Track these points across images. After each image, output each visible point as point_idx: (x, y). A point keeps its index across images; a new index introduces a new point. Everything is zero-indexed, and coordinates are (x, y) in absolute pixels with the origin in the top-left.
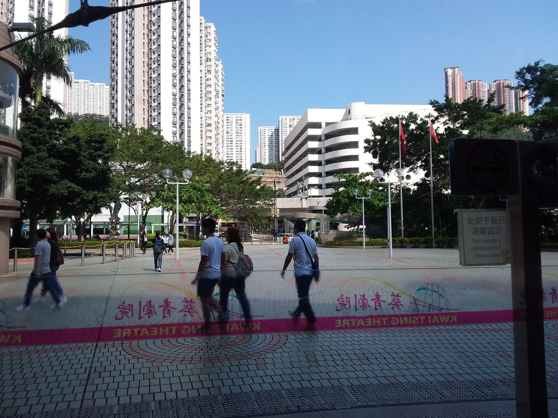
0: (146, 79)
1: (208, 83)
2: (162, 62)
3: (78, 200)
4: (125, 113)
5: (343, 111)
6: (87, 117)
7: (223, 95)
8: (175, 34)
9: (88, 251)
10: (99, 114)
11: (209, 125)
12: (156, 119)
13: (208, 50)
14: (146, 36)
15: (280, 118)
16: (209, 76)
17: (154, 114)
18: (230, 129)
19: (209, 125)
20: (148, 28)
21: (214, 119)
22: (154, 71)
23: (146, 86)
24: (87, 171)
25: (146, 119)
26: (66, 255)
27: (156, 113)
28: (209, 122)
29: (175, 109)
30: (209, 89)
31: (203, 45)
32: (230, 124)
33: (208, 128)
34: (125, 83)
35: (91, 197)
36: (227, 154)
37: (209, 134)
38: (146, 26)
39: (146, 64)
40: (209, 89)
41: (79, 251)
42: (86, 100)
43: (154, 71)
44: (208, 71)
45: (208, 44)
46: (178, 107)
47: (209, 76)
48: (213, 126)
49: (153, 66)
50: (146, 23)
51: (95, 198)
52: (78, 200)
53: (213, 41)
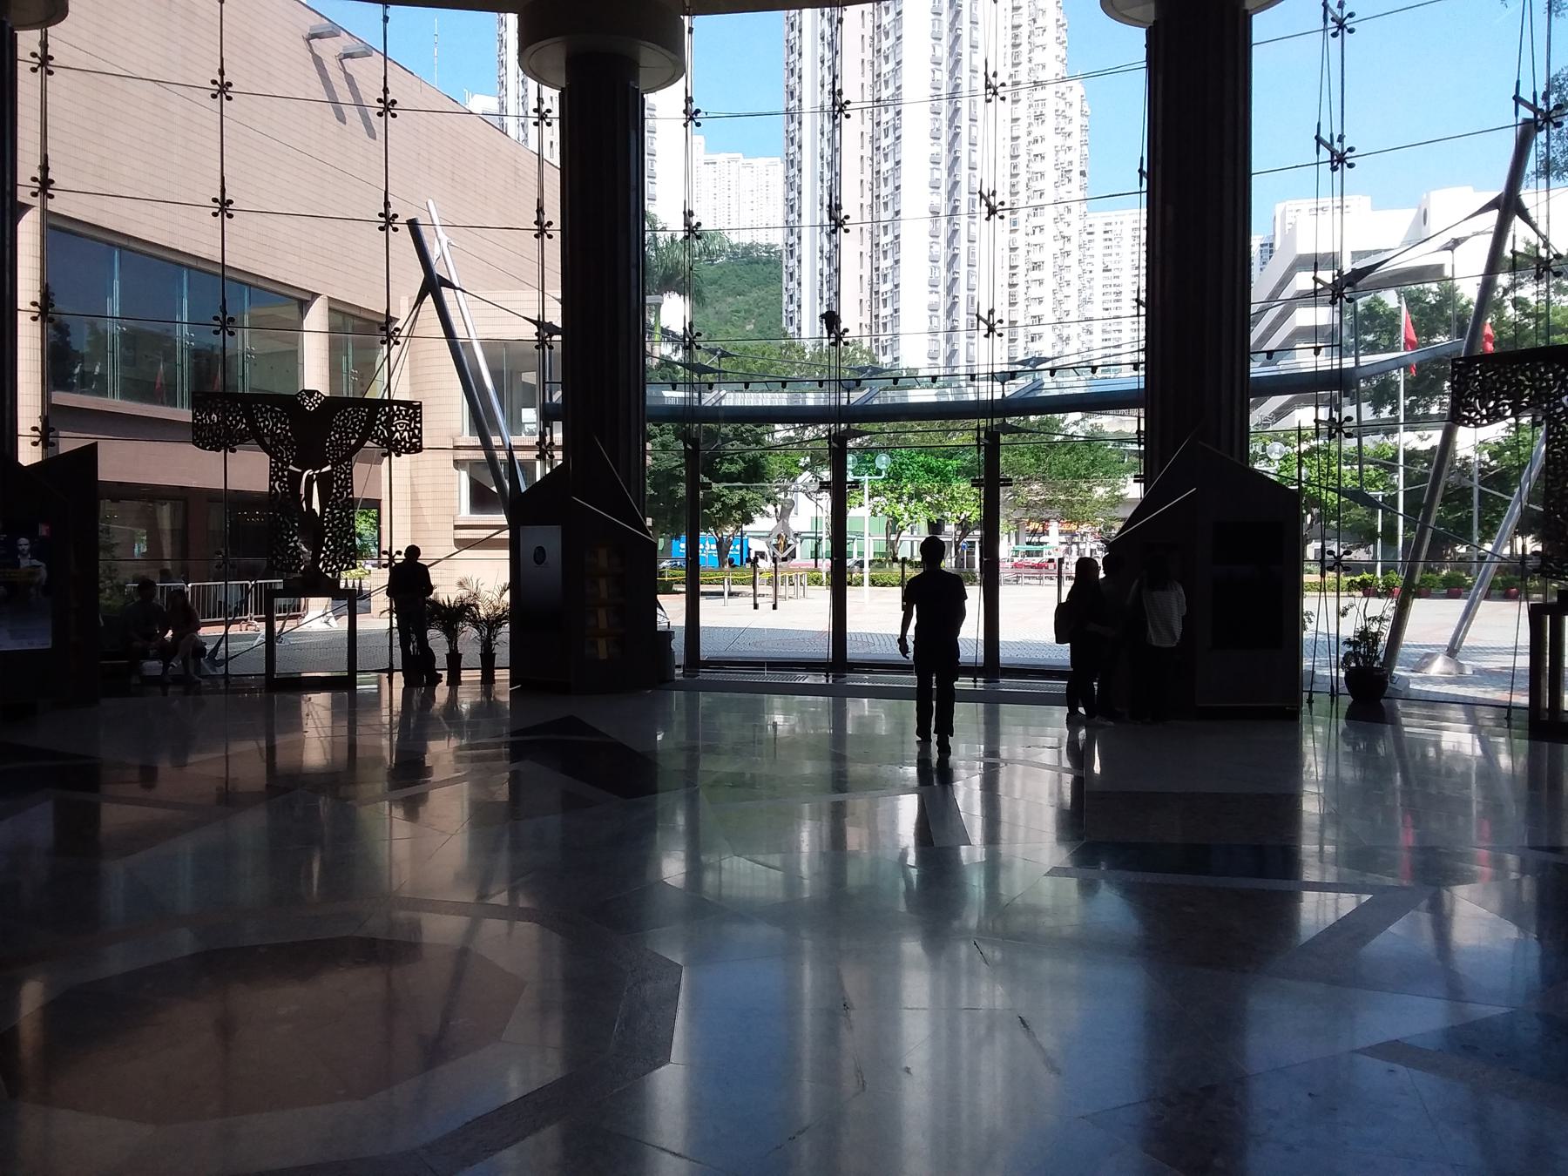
0: (867, 177)
1: (1037, 149)
2: (905, 132)
3: (718, 506)
4: (819, 266)
5: (1410, 214)
6: (735, 254)
7: (1083, 173)
8: (938, 53)
9: (734, 588)
10: (765, 242)
11: (1037, 266)
12: (890, 277)
13: (1038, 56)
14: (867, 66)
15: (1279, 208)
16: (1037, 131)
17: (885, 264)
18: (1114, 257)
19: (1037, 266)
20: (872, 45)
21: (1053, 247)
22: (886, 155)
23: (868, 194)
24: (732, 462)
25: (866, 279)
26: (704, 594)
27: (889, 262)
28: (1035, 257)
29: (936, 247)
30: (1037, 166)
31: (1024, 48)
32: (1114, 243)
33: (1035, 275)
34: (819, 192)
35: (736, 500)
36: (1104, 331)
37: (1035, 291)
38: (867, 41)
39: (867, 138)
40: (1037, 166)
41: (719, 588)
42: (734, 207)
43: (886, 155)
44: (1037, 118)
45: (1038, 41)
46: (942, 240)
47: (1037, 131)
48: (1049, 268)
49: (884, 143)
50: (868, 32)
51: (743, 501)
52: (718, 506)
53: (1052, 32)
